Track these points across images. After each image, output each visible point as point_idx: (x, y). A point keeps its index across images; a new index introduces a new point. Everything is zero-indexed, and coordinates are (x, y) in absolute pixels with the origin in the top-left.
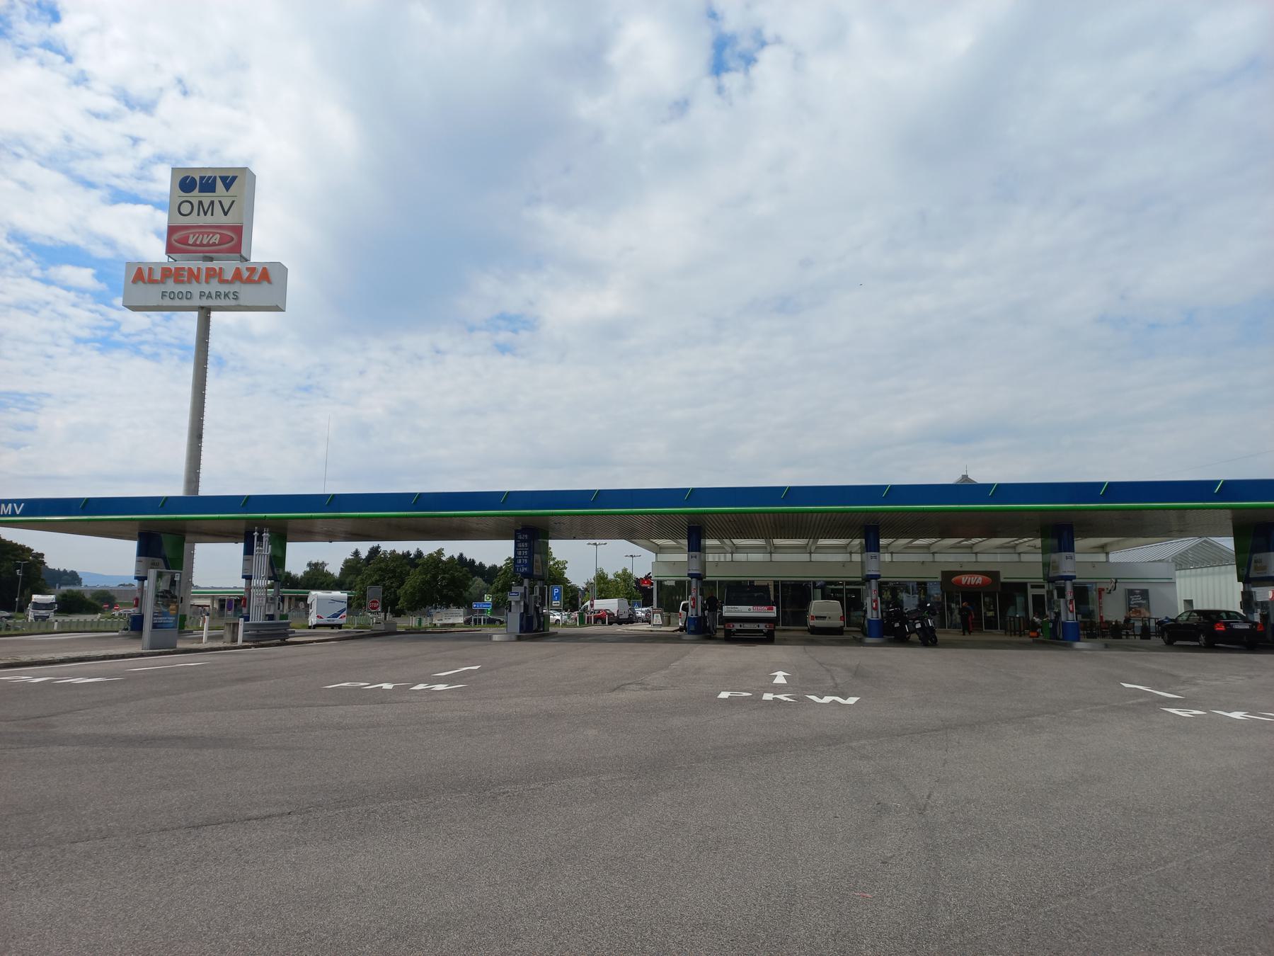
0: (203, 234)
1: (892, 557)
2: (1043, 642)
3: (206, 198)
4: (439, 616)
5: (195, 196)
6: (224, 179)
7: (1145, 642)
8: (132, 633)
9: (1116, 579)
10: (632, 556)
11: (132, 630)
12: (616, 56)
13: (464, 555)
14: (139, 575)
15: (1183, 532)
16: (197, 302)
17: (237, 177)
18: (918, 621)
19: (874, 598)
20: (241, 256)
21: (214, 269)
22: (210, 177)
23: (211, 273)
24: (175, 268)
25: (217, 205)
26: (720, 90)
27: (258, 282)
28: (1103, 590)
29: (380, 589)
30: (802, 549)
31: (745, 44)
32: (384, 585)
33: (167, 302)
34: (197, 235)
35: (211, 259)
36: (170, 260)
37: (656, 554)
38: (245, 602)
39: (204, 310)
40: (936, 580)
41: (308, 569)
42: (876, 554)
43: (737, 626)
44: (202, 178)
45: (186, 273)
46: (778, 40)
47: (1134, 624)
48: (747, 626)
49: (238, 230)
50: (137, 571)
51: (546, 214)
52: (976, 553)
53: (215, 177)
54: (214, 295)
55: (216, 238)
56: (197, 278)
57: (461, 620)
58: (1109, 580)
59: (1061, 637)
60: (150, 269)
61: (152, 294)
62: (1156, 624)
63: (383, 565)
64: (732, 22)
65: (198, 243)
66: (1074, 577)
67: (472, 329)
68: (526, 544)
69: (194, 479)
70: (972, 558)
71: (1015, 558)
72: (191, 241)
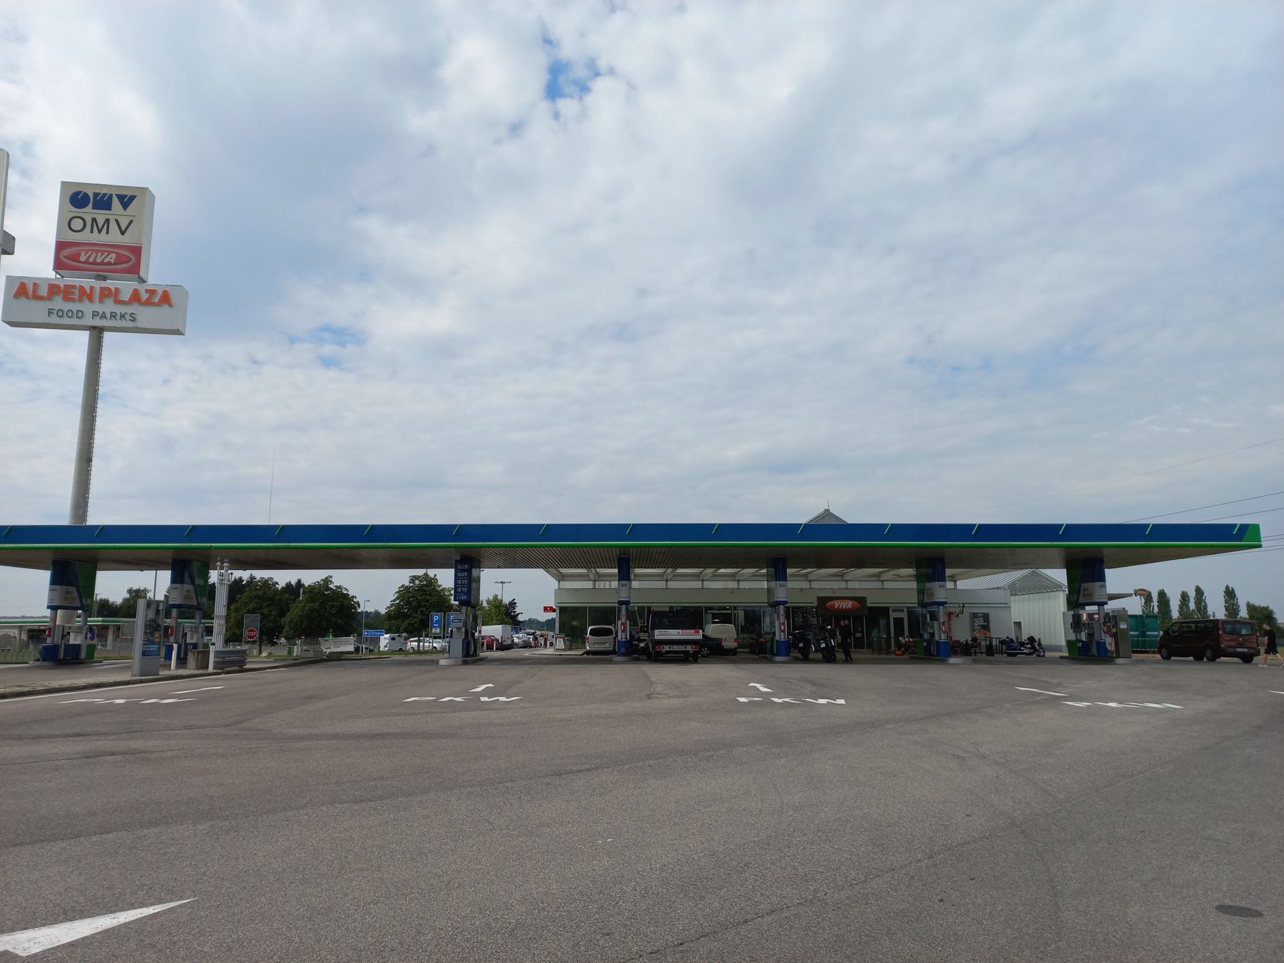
0: (97, 252)
1: (739, 584)
2: (918, 658)
3: (101, 216)
4: (327, 645)
5: (88, 212)
6: (121, 198)
7: (990, 658)
8: (45, 663)
9: (964, 604)
10: (502, 582)
11: (43, 661)
12: (449, 71)
13: (303, 582)
14: (51, 604)
15: (1016, 566)
16: (89, 321)
17: (135, 196)
18: (822, 641)
19: (782, 621)
20: (140, 277)
21: (109, 289)
22: (105, 195)
23: (105, 294)
24: (65, 285)
25: (113, 224)
26: (556, 115)
27: (159, 304)
28: (953, 613)
29: (258, 617)
30: (660, 577)
31: (580, 72)
32: (262, 614)
33: (54, 320)
34: (90, 253)
35: (105, 278)
36: (58, 276)
37: (559, 581)
38: (172, 631)
39: (96, 331)
40: (812, 605)
41: (128, 596)
42: (627, 582)
43: (667, 648)
44: (96, 195)
45: (77, 292)
46: (612, 71)
47: (980, 643)
48: (676, 648)
49: (137, 251)
50: (50, 600)
51: (374, 226)
52: (847, 581)
53: (111, 196)
54: (108, 316)
55: (113, 257)
56: (90, 298)
57: (351, 648)
58: (957, 605)
59: (935, 654)
60: (35, 285)
61: (37, 310)
62: (999, 642)
63: (260, 593)
64: (568, 51)
65: (91, 260)
66: (786, 602)
67: (293, 340)
68: (466, 573)
69: (83, 504)
70: (843, 585)
71: (878, 585)
72: (83, 258)
